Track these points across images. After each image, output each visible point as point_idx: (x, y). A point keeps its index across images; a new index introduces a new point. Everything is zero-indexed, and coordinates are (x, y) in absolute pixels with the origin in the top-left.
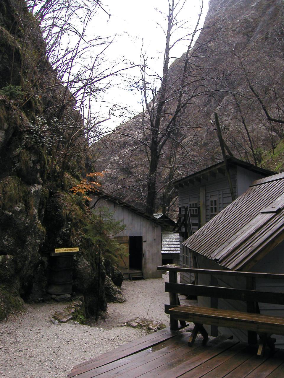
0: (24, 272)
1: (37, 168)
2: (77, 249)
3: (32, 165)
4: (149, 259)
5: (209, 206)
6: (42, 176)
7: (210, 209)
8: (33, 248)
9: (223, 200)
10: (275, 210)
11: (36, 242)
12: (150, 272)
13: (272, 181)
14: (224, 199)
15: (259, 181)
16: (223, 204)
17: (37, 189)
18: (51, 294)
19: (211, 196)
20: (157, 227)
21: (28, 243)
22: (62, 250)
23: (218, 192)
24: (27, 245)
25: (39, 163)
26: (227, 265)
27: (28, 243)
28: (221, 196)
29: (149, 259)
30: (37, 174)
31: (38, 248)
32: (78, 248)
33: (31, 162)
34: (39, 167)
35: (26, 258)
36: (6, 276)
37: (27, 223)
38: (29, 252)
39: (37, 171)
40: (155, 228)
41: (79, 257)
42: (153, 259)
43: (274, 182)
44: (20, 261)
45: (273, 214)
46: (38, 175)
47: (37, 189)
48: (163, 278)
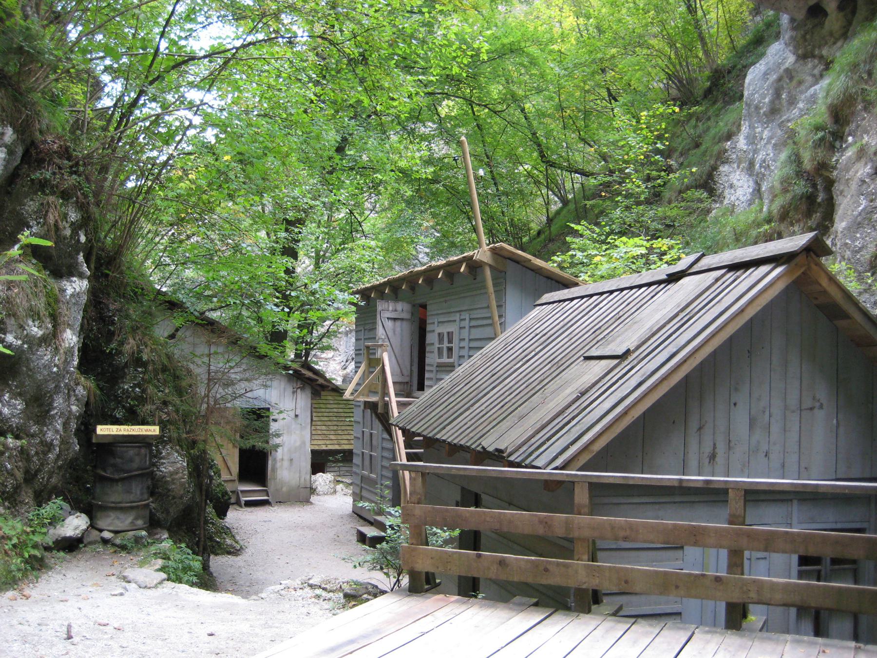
0: (43, 478)
1: (79, 240)
2: (154, 430)
3: (68, 232)
4: (282, 459)
5: (433, 344)
6: (87, 260)
7: (436, 351)
8: (66, 425)
9: (469, 331)
10: (620, 351)
11: (70, 412)
12: (284, 489)
17: (78, 290)
18: (101, 531)
19: (439, 322)
21: (56, 411)
22: (115, 430)
23: (458, 315)
26: (532, 458)
27: (56, 411)
28: (466, 323)
29: (282, 459)
30: (78, 254)
31: (73, 425)
33: (67, 225)
34: (83, 239)
35: (50, 446)
36: (6, 486)
37: (55, 365)
38: (57, 431)
39: (77, 247)
40: (299, 391)
41: (164, 447)
42: (291, 460)
44: (37, 453)
45: (616, 361)
46: (81, 258)
48: (312, 503)
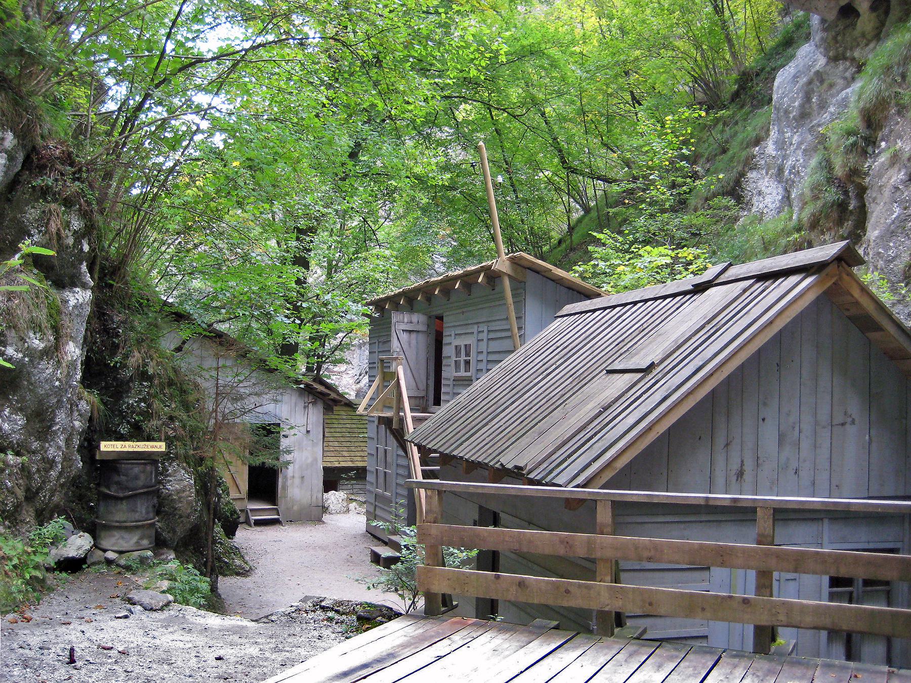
0: (44, 497)
1: (82, 249)
2: (160, 446)
3: (70, 241)
5: (450, 357)
8: (68, 441)
10: (644, 365)
11: (73, 427)
12: (295, 508)
13: (594, 311)
14: (490, 342)
15: (568, 306)
16: (488, 353)
17: (81, 301)
18: (105, 551)
20: (314, 403)
21: (58, 427)
22: (119, 446)
23: (476, 327)
24: (55, 432)
25: (86, 239)
26: (553, 475)
27: (58, 427)
28: (484, 336)
30: (82, 264)
31: (76, 442)
32: (163, 444)
34: (86, 248)
35: (52, 463)
36: (7, 504)
38: (59, 448)
39: (80, 256)
40: (310, 405)
42: (303, 477)
43: (618, 309)
44: (38, 470)
46: (84, 267)
47: (81, 301)
48: (324, 523)
